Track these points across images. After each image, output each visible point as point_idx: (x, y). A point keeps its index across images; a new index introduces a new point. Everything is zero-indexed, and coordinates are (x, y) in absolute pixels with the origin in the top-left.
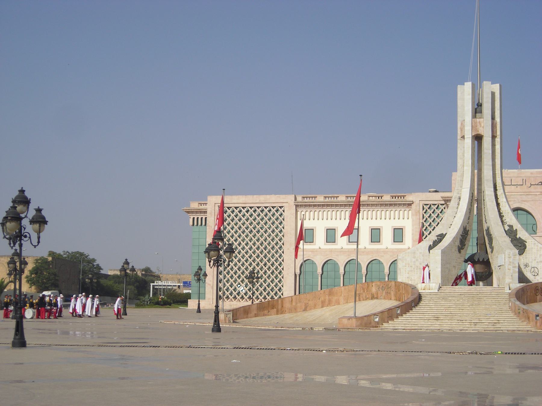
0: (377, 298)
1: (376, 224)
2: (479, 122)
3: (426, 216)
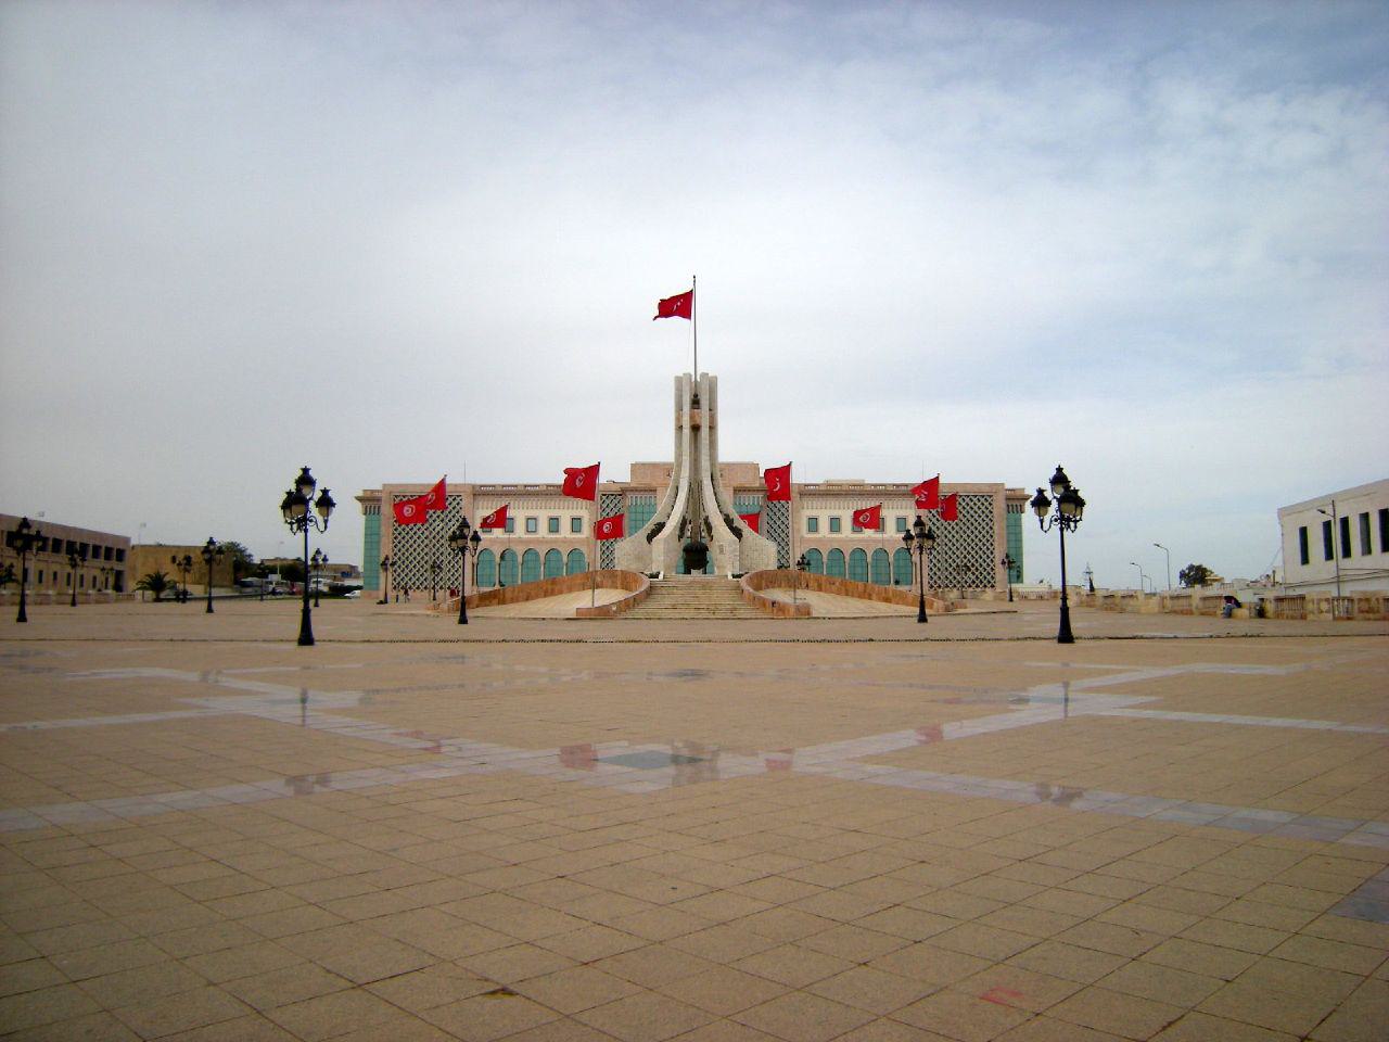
0: (602, 587)
3: (604, 506)
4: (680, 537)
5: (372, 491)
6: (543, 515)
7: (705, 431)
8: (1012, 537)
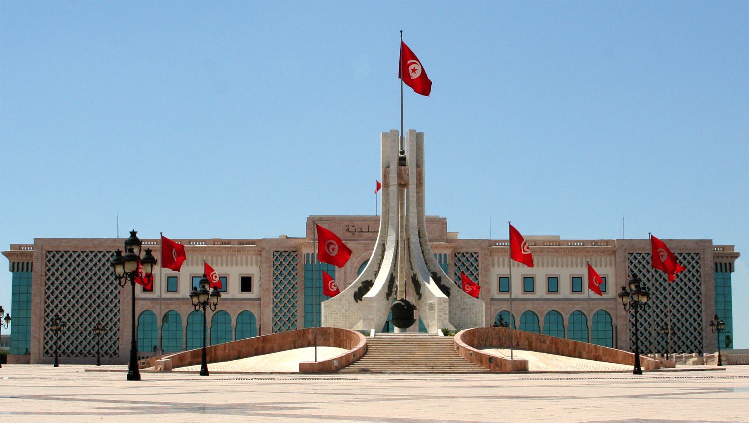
1: (553, 271)
2: (405, 169)
3: (277, 263)
4: (389, 295)
5: (20, 246)
7: (413, 186)
8: (720, 299)
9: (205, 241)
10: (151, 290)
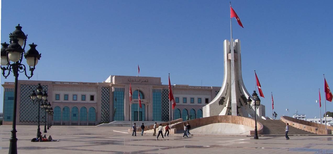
6: (79, 94)
9: (78, 83)
10: (68, 100)
